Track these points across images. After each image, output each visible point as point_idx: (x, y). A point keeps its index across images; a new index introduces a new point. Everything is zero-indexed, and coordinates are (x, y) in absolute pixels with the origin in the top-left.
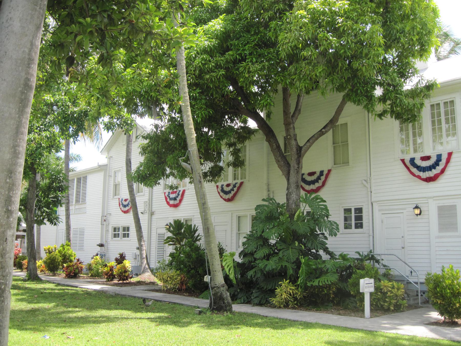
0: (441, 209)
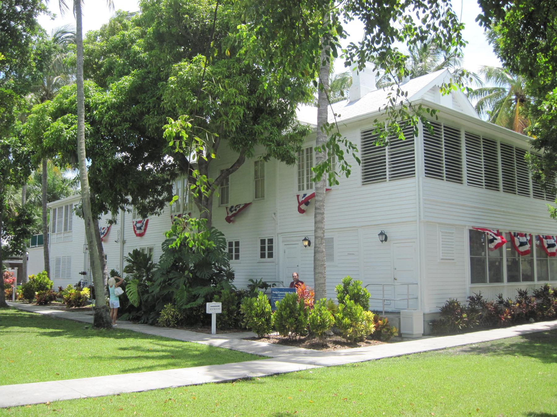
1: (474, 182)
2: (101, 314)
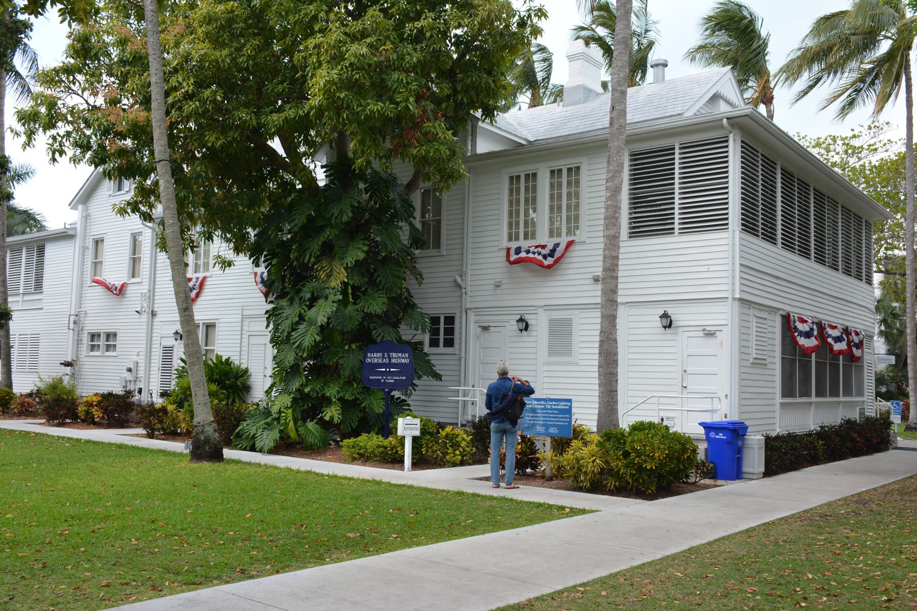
0: (553, 323)
1: (788, 245)
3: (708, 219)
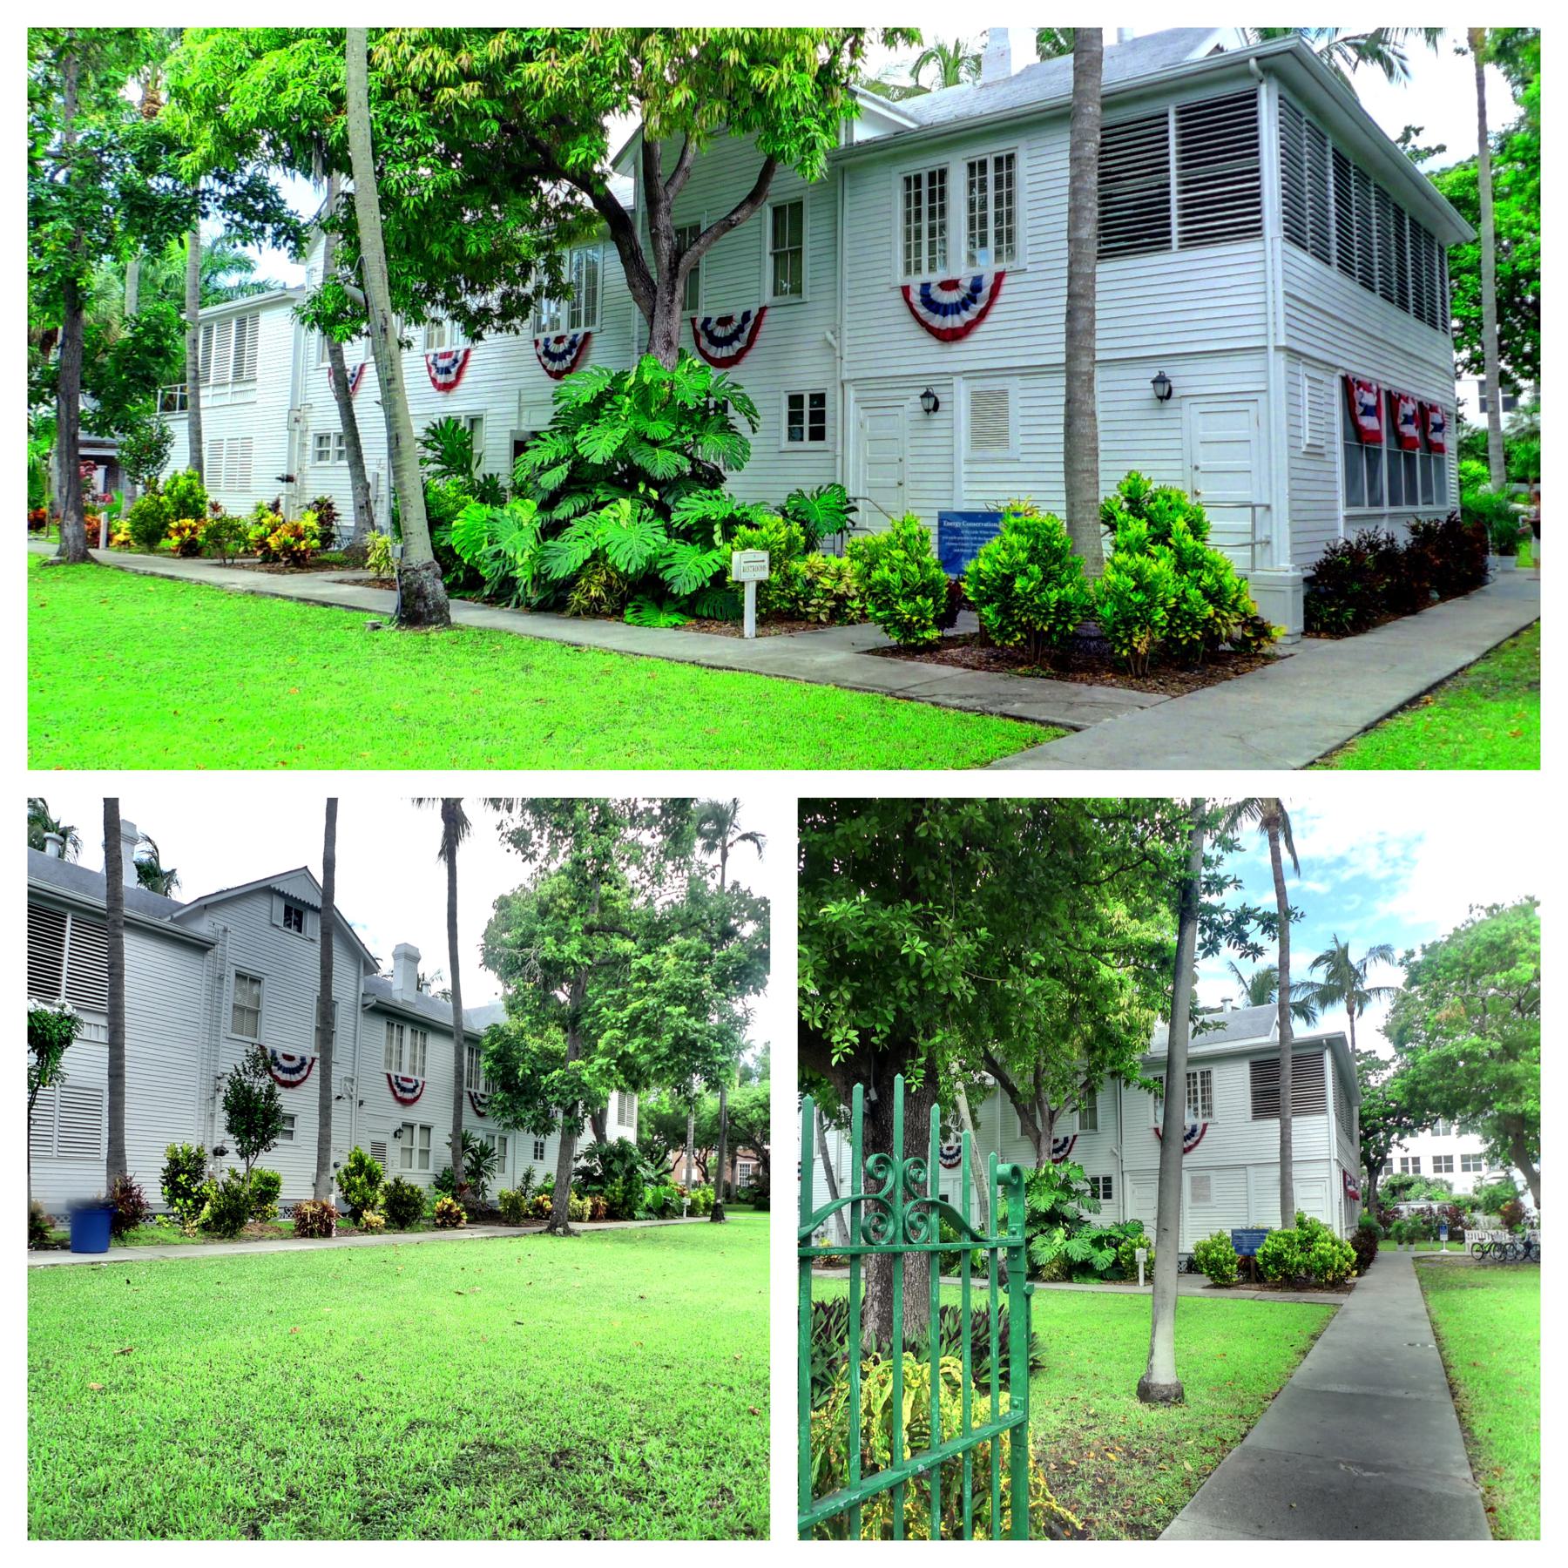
0: (977, 397)
2: (422, 586)
3: (630, 1125)
